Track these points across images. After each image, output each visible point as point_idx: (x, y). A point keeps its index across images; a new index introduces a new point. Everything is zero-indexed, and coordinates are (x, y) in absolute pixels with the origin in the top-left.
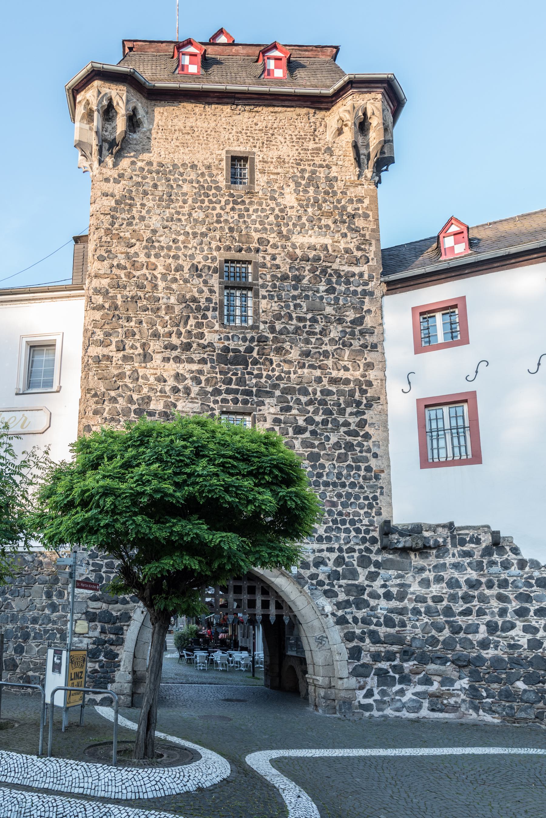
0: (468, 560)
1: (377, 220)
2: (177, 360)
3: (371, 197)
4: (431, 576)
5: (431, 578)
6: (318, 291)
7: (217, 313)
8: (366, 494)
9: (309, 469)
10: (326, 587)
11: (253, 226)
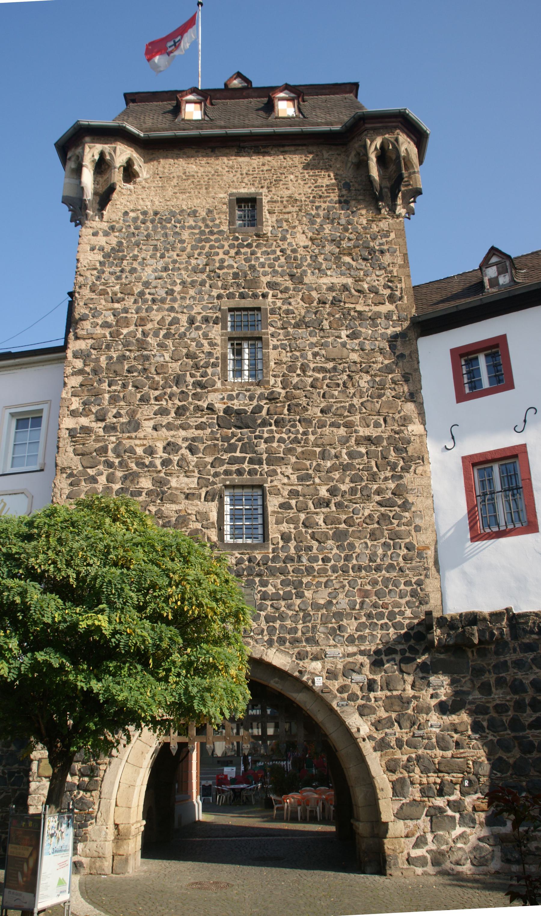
0: (530, 656)
1: (405, 255)
2: (169, 427)
3: (397, 230)
4: (492, 678)
5: (492, 681)
6: (340, 337)
7: (219, 369)
8: (408, 579)
9: (335, 551)
10: (360, 702)
11: (262, 270)
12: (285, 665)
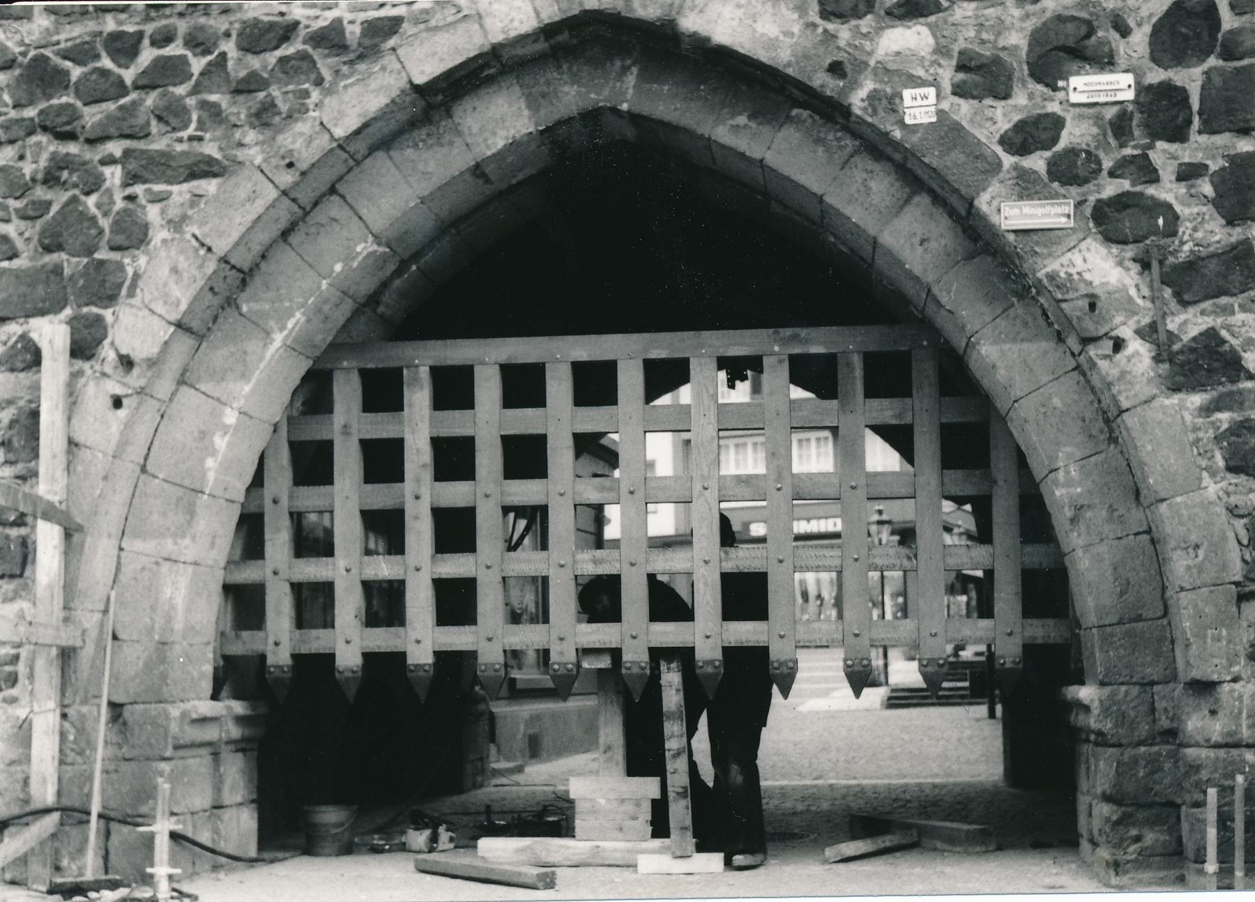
12: (772, 44)
